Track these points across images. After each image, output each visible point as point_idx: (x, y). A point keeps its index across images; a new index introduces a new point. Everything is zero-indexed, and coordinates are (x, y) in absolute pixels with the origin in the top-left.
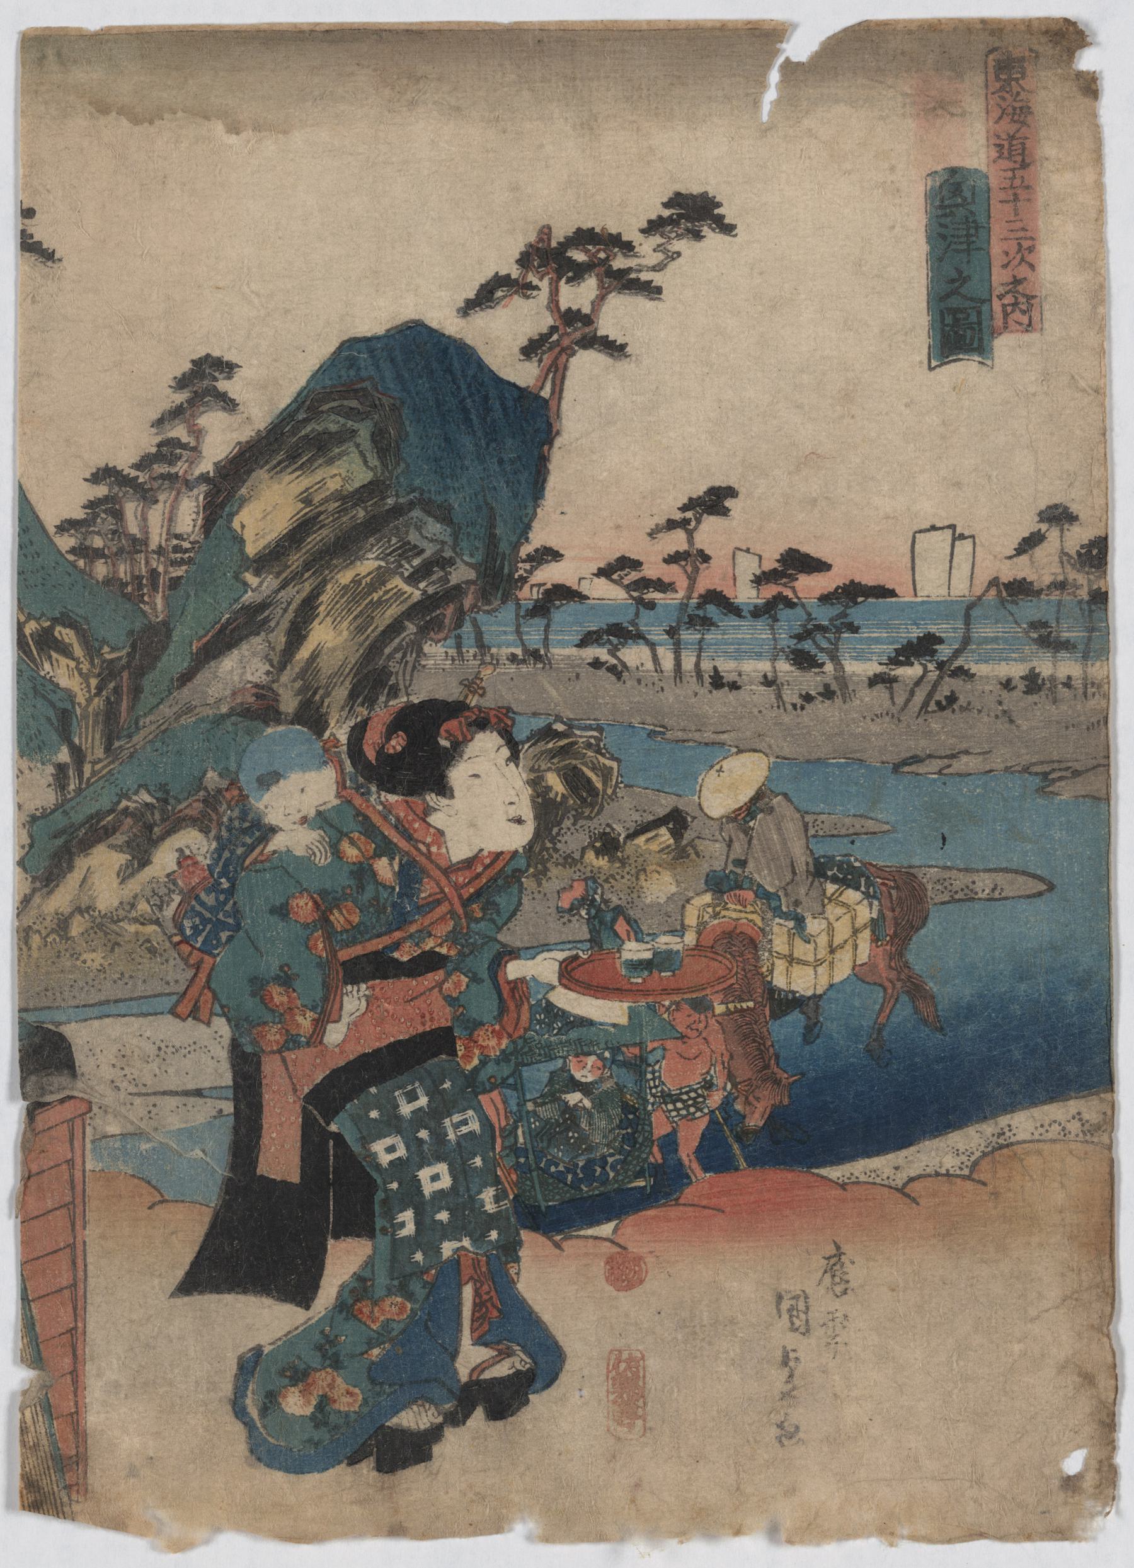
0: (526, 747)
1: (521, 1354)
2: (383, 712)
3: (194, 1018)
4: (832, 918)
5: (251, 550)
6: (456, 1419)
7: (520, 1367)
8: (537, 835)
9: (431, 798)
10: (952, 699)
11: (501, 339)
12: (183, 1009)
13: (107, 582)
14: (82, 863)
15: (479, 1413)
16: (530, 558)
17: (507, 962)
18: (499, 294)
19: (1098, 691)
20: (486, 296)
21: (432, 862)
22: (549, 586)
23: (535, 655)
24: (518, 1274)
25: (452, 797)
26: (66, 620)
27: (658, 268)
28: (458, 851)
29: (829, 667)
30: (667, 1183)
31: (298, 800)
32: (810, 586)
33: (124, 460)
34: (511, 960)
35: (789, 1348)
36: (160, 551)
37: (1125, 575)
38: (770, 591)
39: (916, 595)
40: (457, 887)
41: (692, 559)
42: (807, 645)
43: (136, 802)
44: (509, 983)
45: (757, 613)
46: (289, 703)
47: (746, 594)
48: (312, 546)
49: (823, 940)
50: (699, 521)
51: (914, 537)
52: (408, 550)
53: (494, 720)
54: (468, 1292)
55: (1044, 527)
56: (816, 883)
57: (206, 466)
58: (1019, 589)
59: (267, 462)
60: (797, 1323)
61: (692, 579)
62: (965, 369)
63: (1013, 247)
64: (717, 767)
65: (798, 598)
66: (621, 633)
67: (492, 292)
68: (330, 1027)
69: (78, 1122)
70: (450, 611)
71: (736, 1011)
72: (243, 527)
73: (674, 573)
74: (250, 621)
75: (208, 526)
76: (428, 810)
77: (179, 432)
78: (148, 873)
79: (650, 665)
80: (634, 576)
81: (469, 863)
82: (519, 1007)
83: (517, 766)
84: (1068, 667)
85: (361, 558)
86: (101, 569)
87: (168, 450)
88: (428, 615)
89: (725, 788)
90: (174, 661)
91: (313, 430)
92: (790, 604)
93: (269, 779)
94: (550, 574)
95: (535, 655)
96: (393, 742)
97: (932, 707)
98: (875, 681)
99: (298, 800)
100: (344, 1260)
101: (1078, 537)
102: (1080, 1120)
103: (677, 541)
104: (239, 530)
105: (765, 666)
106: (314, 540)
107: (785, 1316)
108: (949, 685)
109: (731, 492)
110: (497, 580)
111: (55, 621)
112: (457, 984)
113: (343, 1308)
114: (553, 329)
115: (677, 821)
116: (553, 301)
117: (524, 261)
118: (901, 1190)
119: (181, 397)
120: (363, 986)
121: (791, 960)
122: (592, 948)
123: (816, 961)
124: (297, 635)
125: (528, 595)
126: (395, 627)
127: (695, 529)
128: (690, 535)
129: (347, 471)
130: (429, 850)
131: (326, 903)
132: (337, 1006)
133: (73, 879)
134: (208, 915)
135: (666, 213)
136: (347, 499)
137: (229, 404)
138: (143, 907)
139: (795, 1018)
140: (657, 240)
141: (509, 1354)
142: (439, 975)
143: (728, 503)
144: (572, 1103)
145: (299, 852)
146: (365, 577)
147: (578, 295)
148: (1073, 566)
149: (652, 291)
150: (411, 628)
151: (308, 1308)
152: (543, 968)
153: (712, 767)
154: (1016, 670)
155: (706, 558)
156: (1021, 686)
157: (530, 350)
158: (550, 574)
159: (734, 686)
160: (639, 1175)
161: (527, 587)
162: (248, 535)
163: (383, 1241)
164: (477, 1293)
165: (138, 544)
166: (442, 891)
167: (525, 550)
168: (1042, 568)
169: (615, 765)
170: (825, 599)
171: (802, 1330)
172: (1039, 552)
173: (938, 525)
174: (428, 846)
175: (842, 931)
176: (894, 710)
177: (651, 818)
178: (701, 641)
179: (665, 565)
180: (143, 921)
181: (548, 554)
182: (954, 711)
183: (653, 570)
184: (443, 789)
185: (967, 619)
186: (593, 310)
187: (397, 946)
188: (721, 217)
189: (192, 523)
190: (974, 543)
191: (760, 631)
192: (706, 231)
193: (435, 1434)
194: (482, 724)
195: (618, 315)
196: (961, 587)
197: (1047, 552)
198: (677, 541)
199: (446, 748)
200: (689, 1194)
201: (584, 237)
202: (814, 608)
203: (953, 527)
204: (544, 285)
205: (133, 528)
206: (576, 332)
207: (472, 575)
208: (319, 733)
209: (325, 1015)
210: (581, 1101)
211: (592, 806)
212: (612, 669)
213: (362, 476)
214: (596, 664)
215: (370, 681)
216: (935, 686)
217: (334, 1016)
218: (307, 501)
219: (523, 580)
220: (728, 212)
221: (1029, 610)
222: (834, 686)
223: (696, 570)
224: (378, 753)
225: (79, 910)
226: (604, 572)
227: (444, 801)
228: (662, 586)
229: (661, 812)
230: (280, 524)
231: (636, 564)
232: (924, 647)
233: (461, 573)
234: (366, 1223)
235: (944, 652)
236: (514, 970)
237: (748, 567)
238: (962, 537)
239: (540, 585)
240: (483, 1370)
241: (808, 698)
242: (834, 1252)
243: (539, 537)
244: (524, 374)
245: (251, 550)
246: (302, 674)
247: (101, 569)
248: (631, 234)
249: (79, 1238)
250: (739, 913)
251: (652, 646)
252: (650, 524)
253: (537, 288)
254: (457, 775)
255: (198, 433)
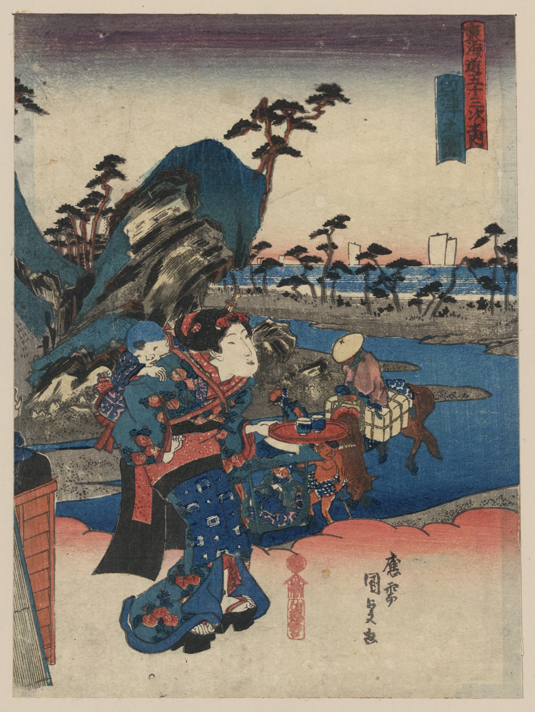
0: (255, 329)
1: (250, 601)
2: (189, 317)
3: (105, 450)
4: (392, 408)
5: (132, 242)
6: (221, 630)
7: (249, 607)
8: (261, 368)
9: (212, 353)
10: (446, 311)
11: (245, 149)
12: (100, 446)
13: (67, 256)
14: (55, 382)
15: (231, 628)
16: (256, 247)
17: (246, 425)
18: (242, 129)
19: (511, 308)
20: (239, 129)
21: (212, 381)
22: (265, 259)
23: (259, 290)
24: (249, 565)
25: (221, 352)
26: (47, 273)
27: (315, 117)
28: (224, 376)
29: (391, 296)
30: (314, 526)
31: (152, 353)
32: (382, 260)
33: (74, 202)
34: (248, 425)
35: (371, 599)
36: (90, 243)
37: (523, 259)
38: (364, 261)
39: (430, 264)
40: (223, 393)
41: (330, 247)
42: (382, 286)
43: (80, 353)
44: (246, 435)
45: (359, 271)
46: (148, 309)
47: (353, 263)
48: (159, 241)
49: (387, 418)
50: (333, 231)
51: (429, 239)
52: (202, 242)
53: (240, 318)
54: (226, 572)
55: (488, 235)
56: (384, 392)
57: (111, 204)
58: (475, 263)
59: (138, 204)
60: (374, 588)
61: (330, 256)
62: (453, 165)
63: (474, 111)
64: (340, 340)
65: (378, 265)
66: (296, 281)
67: (240, 128)
68: (166, 454)
69: (51, 495)
70: (221, 269)
71: (348, 448)
72: (128, 231)
73: (322, 254)
74: (129, 273)
75: (111, 232)
76: (210, 358)
77: (99, 188)
78: (83, 386)
79: (310, 293)
80: (304, 255)
81: (229, 382)
82: (251, 446)
83: (250, 339)
84: (499, 297)
85: (182, 244)
86: (65, 251)
87: (94, 197)
88: (212, 272)
89: (347, 347)
90: (99, 288)
91: (160, 188)
92: (373, 268)
93: (140, 345)
94: (266, 253)
95: (259, 290)
96: (195, 327)
97: (437, 314)
98: (412, 302)
99: (152, 353)
100: (171, 558)
101: (502, 240)
102: (502, 498)
103: (322, 239)
104: (126, 233)
105: (362, 295)
106: (158, 240)
107: (369, 586)
108: (444, 305)
109: (348, 218)
110: (241, 258)
111: (43, 273)
112: (223, 435)
113: (172, 578)
114: (267, 145)
115: (322, 364)
116: (268, 131)
117: (254, 114)
118: (422, 529)
119: (99, 173)
120: (181, 436)
121: (373, 426)
122: (283, 420)
123: (384, 426)
124: (153, 278)
125: (256, 262)
126: (196, 276)
127: (332, 233)
128: (329, 236)
129: (179, 206)
130: (211, 376)
131: (166, 396)
132: (169, 444)
133: (52, 387)
134: (112, 402)
135: (318, 93)
136: (177, 220)
137: (122, 177)
138: (82, 399)
139: (375, 452)
140: (314, 105)
141: (245, 601)
142: (215, 431)
143: (346, 223)
144: (274, 488)
145: (153, 375)
146: (54, 364)
147: (279, 130)
148: (501, 252)
149: (313, 129)
150: (204, 277)
151: (154, 580)
152: (262, 429)
153: (338, 340)
154: (475, 298)
155: (336, 247)
156: (477, 305)
157: (256, 155)
158: (266, 253)
159: (348, 304)
160: (302, 521)
161: (256, 259)
162: (130, 235)
163: (190, 550)
164: (230, 574)
165: (81, 239)
166: (217, 394)
167: (255, 243)
168: (487, 252)
169: (294, 338)
170: (389, 266)
171: (376, 591)
172: (485, 246)
173: (440, 233)
174: (210, 374)
175: (396, 413)
176: (421, 315)
177: (310, 362)
178: (334, 283)
179: (317, 251)
180: (81, 406)
181: (265, 245)
182: (447, 317)
183: (312, 252)
184: (218, 349)
185: (454, 276)
186: (285, 136)
187: (195, 418)
188: (343, 96)
189: (105, 230)
190: (456, 242)
191: (360, 279)
192: (336, 102)
193: (212, 637)
194: (235, 319)
195: (297, 139)
196: (450, 261)
197: (490, 245)
198: (322, 239)
199: (219, 330)
200: (326, 530)
201: (281, 104)
202: (382, 272)
203: (447, 234)
204: (263, 125)
205: (79, 233)
206: (277, 147)
207: (231, 253)
208: (161, 325)
209: (164, 447)
210: (278, 488)
211: (284, 357)
212: (293, 297)
213: (184, 209)
214: (286, 294)
215: (185, 300)
216: (438, 306)
217: (168, 449)
218: (156, 220)
219: (254, 256)
220: (346, 94)
221: (480, 273)
222: (393, 305)
223: (332, 252)
224: (188, 332)
225: (54, 401)
226: (291, 253)
227: (218, 354)
228: (317, 259)
229: (316, 359)
230: (147, 228)
231: (305, 250)
232: (434, 287)
233: (226, 253)
234: (191, 535)
235: (443, 289)
236: (249, 429)
237: (355, 251)
238: (451, 239)
239: (261, 258)
240: (234, 608)
241: (381, 310)
242: (391, 556)
243: (260, 237)
244: (255, 164)
245: (132, 242)
246: (154, 297)
247: (65, 251)
248: (302, 103)
249: (52, 548)
250: (352, 405)
251: (312, 286)
252: (310, 232)
253: (260, 127)
254: (224, 343)
255: (108, 189)
